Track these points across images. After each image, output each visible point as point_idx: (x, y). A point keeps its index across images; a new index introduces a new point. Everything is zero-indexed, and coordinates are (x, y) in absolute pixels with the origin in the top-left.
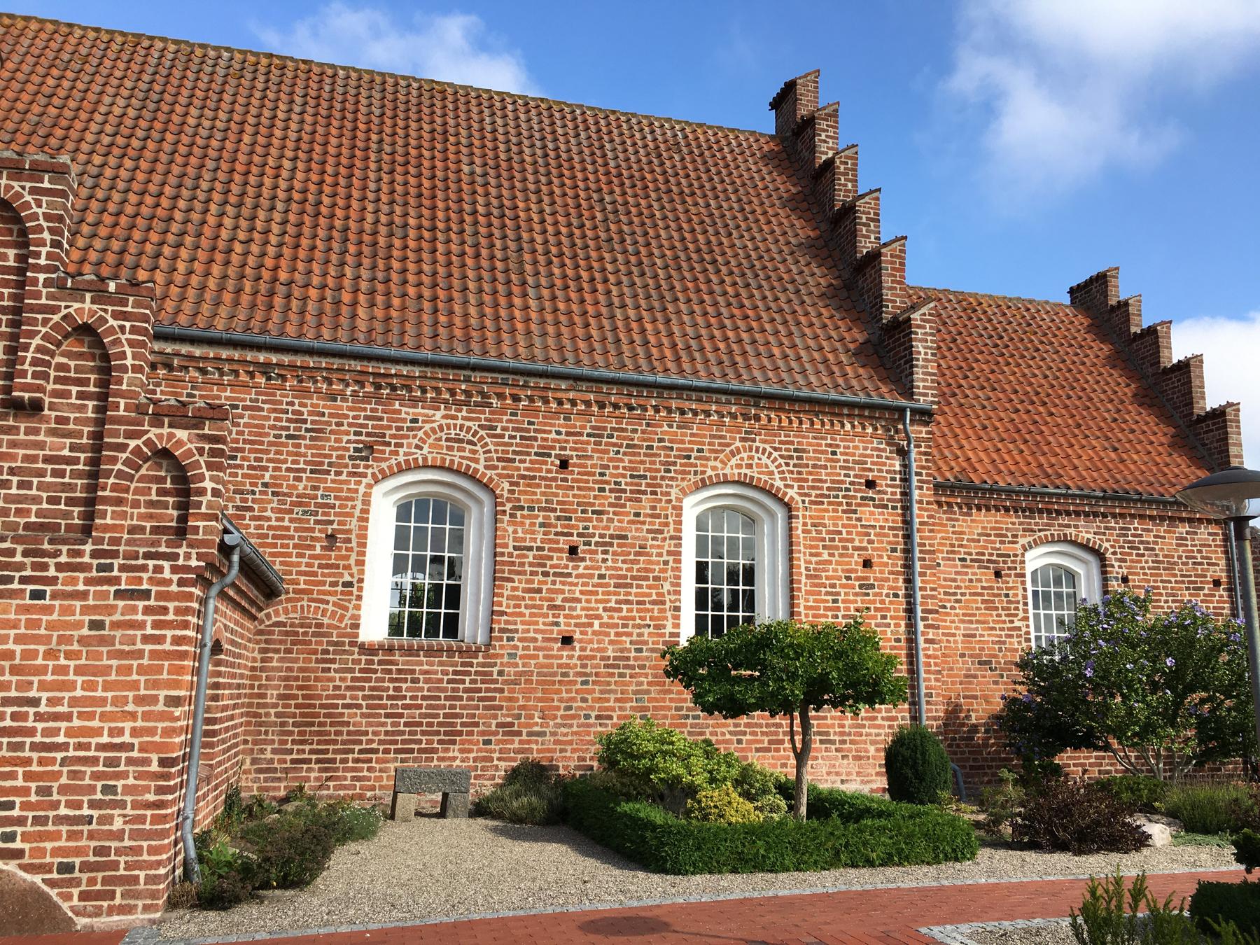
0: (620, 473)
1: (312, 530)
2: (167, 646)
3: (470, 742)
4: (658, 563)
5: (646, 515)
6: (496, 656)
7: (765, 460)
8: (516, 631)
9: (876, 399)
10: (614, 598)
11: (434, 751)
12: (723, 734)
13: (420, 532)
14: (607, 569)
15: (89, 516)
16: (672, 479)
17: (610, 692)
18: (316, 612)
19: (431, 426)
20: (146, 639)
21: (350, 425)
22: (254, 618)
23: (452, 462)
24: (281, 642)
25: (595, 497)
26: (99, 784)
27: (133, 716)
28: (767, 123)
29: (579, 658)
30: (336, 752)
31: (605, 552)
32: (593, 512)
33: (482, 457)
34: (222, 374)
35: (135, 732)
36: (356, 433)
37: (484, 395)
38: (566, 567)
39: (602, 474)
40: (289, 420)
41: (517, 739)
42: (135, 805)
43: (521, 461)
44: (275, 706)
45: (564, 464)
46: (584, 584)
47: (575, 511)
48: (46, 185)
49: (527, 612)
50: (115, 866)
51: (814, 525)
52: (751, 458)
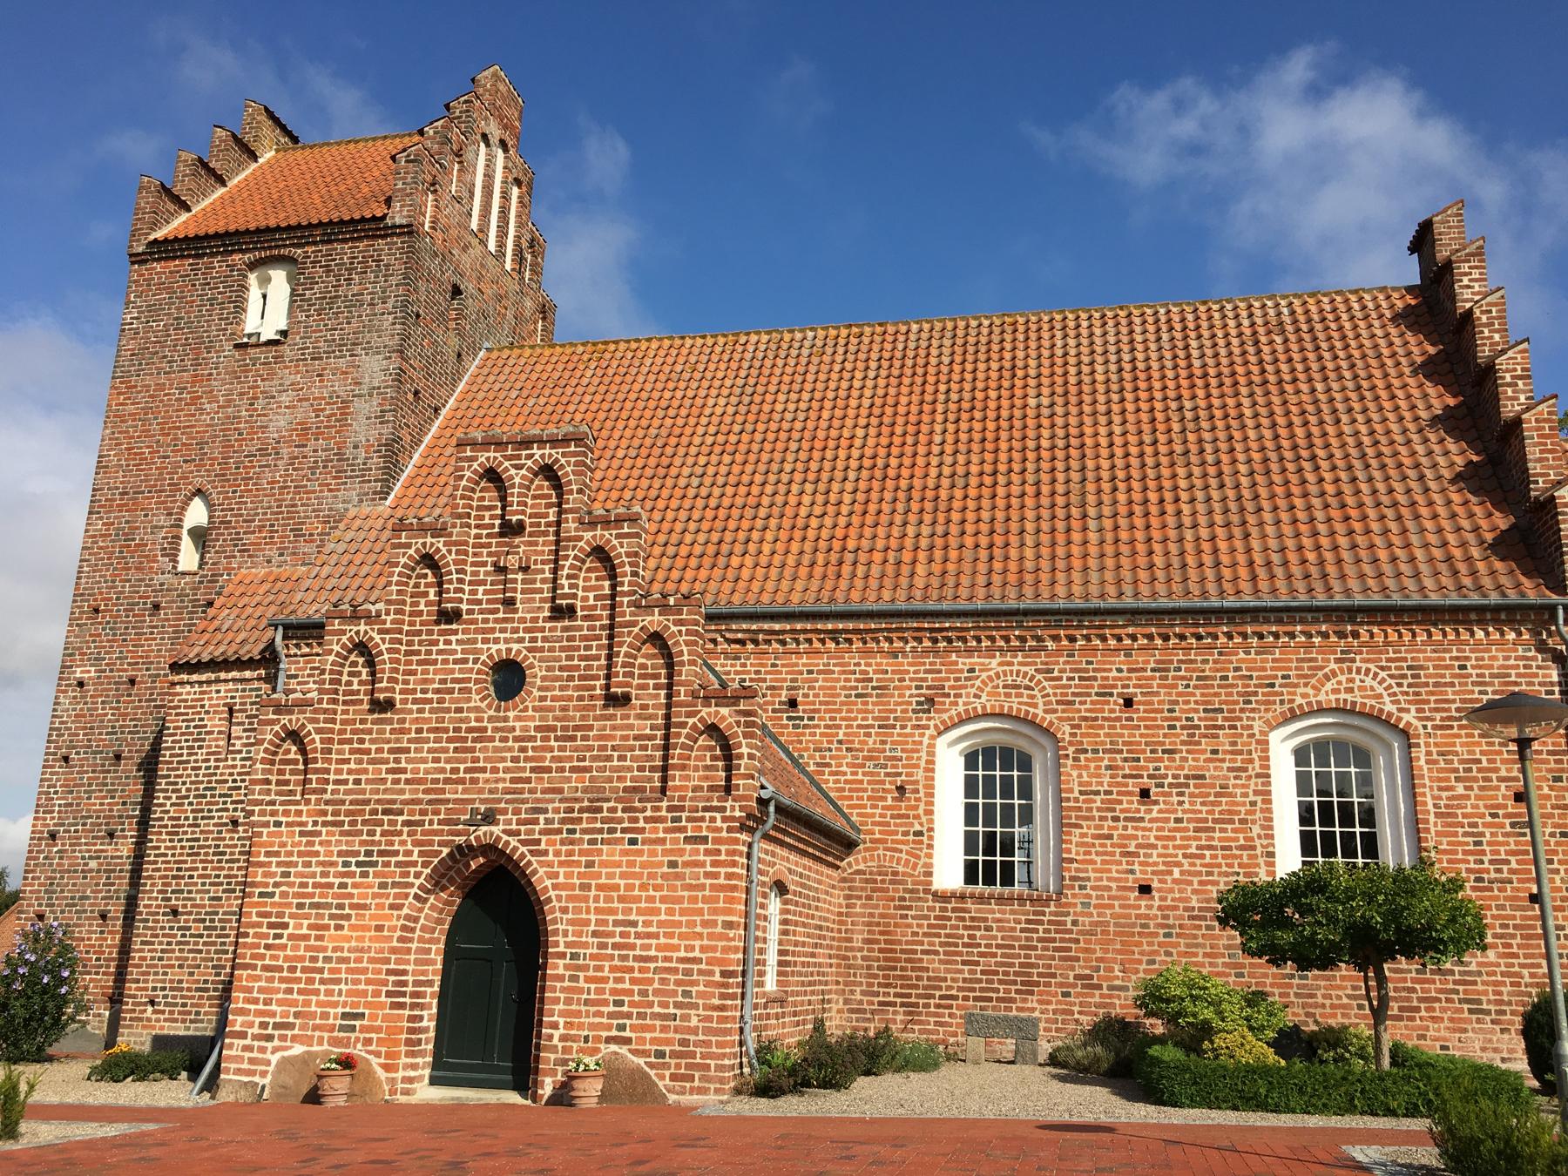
0: (1192, 706)
1: (883, 782)
2: (722, 881)
3: (1048, 993)
4: (1244, 804)
5: (1225, 752)
6: (1068, 905)
7: (1369, 681)
8: (1088, 879)
9: (1513, 597)
10: (1194, 844)
11: (1012, 1000)
12: (1339, 997)
13: (989, 780)
14: (1184, 812)
15: (664, 780)
16: (1253, 710)
17: (1197, 946)
18: (891, 861)
19: (992, 677)
20: (707, 875)
21: (911, 680)
22: (838, 868)
23: (1011, 708)
24: (862, 889)
25: (1165, 735)
26: (680, 989)
27: (700, 936)
28: (1411, 272)
29: (1160, 908)
30: (918, 996)
31: (1181, 794)
32: (1164, 752)
33: (1040, 701)
34: (798, 643)
35: (703, 949)
36: (917, 687)
37: (1039, 639)
38: (1138, 811)
39: (1170, 711)
40: (857, 680)
41: (1097, 992)
42: (706, 1007)
43: (1081, 703)
44: (861, 949)
45: (1128, 703)
46: (1159, 829)
47: (1144, 752)
48: (626, 530)
49: (1098, 859)
50: (693, 1055)
51: (1440, 754)
52: (1352, 680)
